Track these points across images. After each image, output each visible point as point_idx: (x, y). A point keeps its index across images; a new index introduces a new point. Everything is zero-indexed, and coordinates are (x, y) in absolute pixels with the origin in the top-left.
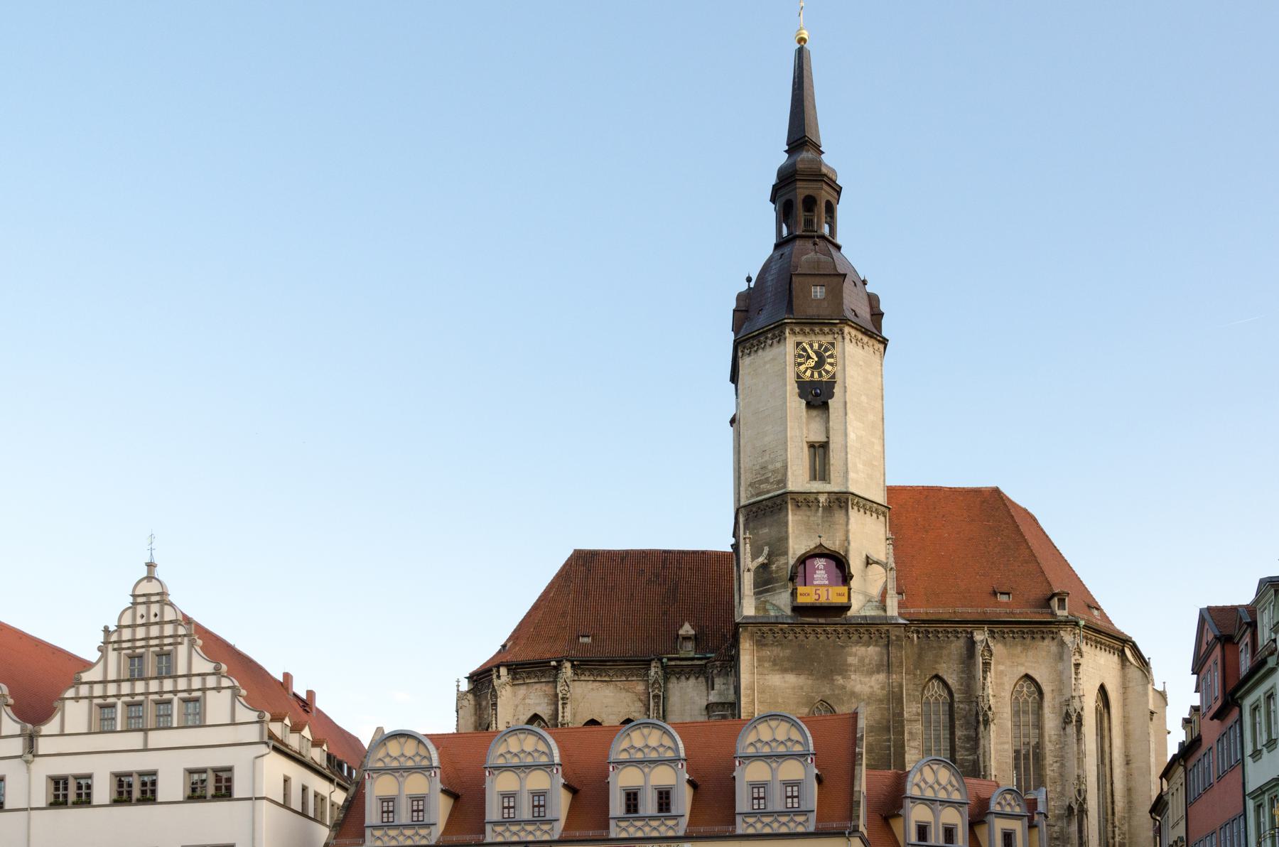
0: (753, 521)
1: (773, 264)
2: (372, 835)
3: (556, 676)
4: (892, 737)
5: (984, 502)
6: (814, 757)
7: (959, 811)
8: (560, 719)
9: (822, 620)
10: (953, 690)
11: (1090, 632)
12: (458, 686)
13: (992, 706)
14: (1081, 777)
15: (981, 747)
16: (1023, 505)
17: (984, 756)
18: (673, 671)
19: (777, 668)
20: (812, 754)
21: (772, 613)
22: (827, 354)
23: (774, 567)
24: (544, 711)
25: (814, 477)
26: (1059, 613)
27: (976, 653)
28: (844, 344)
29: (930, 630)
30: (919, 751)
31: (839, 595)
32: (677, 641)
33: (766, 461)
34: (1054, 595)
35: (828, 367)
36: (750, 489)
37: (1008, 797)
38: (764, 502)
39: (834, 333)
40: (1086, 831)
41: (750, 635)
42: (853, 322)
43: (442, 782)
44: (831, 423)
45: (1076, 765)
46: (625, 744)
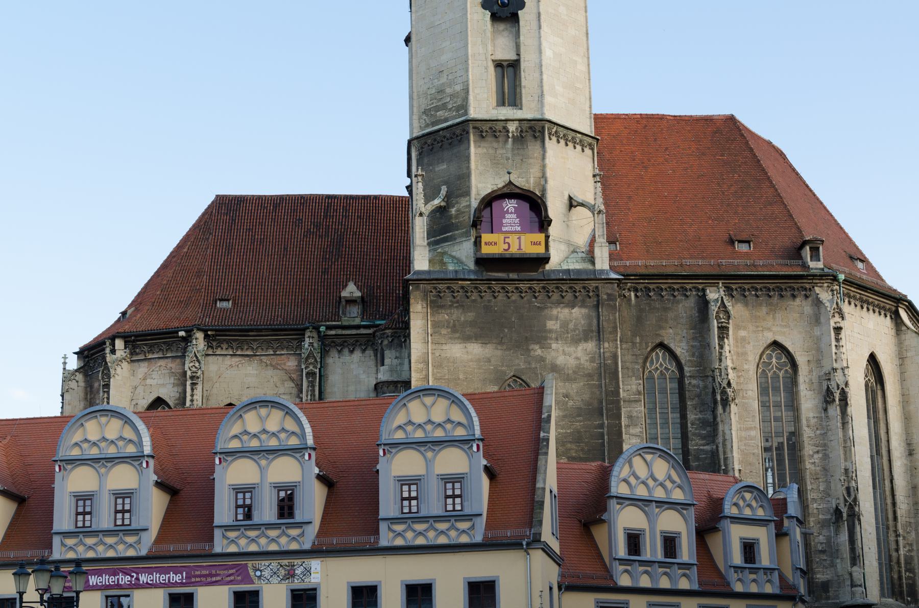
2: (63, 544)
3: (185, 350)
5: (716, 132)
9: (513, 276)
10: (683, 362)
11: (853, 289)
12: (65, 363)
13: (731, 381)
14: (850, 470)
15: (721, 433)
16: (766, 137)
17: (724, 445)
18: (333, 342)
19: (457, 335)
20: (478, 439)
21: (451, 267)
23: (453, 211)
24: (169, 393)
25: (501, 102)
26: (812, 264)
27: (710, 316)
29: (651, 286)
31: (535, 244)
32: (339, 305)
33: (443, 83)
34: (805, 243)
37: (748, 496)
38: (441, 133)
40: (859, 534)
44: (522, 38)
45: (842, 456)
46: (236, 429)
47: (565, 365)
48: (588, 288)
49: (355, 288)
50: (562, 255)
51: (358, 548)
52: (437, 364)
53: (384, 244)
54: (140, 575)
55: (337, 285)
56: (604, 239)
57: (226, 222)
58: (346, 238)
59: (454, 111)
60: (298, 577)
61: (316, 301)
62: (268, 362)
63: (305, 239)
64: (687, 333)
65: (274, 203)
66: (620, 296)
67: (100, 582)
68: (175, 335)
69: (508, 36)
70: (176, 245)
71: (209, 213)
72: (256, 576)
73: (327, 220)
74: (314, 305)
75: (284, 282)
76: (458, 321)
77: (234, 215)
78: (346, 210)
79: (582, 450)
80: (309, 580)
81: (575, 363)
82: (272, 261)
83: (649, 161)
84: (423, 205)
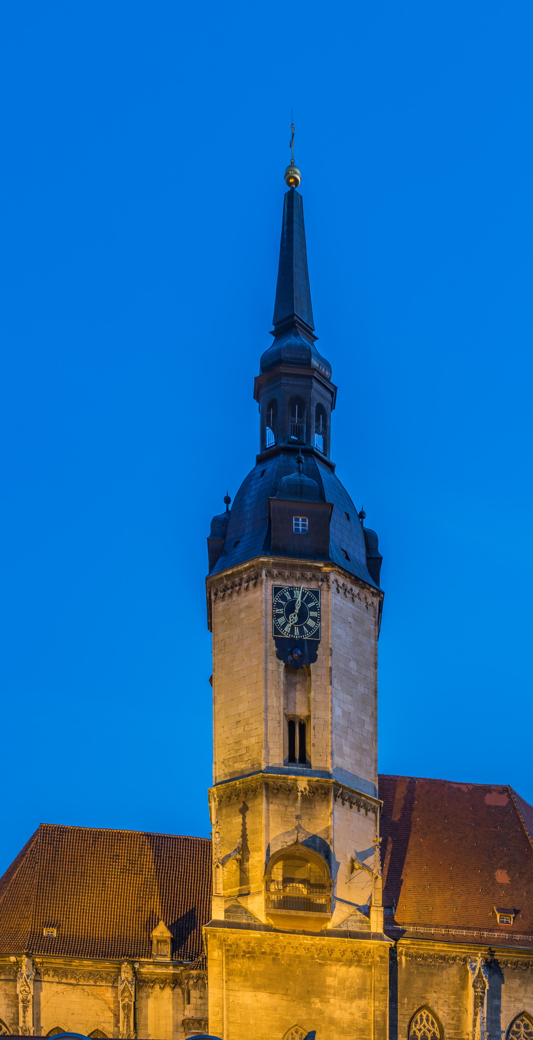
0: (227, 806)
8: (21, 1024)
10: (444, 1024)
19: (248, 984)
22: (310, 605)
35: (310, 622)
47: (341, 1019)
49: (165, 928)
62: (89, 991)
81: (350, 1017)
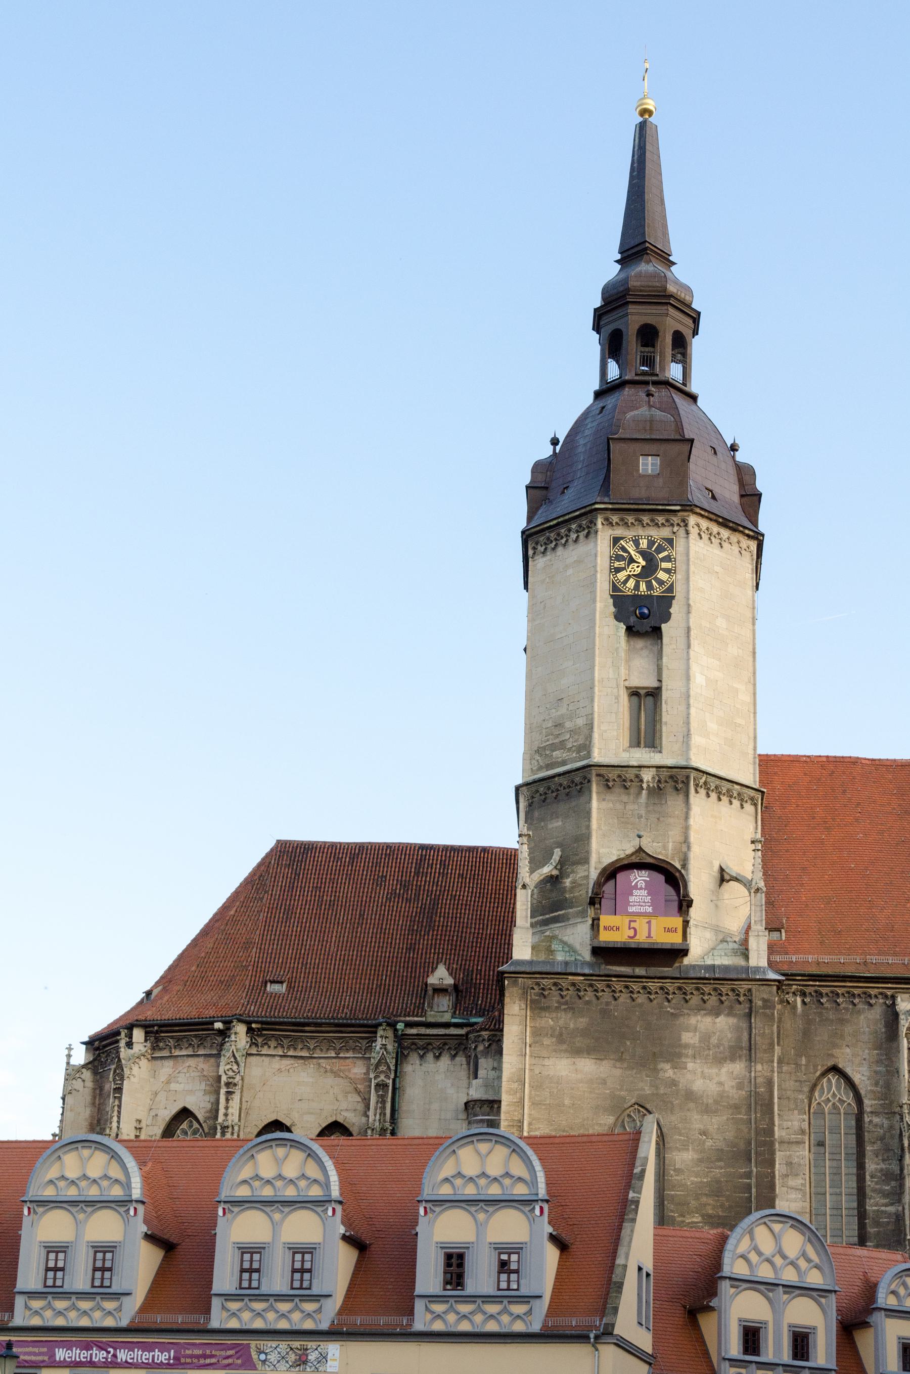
1: (588, 420)
2: (27, 1307)
4: (755, 1170)
6: (546, 1207)
7: (820, 1304)
8: (221, 1118)
9: (640, 971)
10: (863, 1092)
12: (69, 1056)
18: (413, 1044)
19: (564, 1047)
20: (542, 1200)
21: (560, 957)
22: (661, 556)
23: (567, 882)
24: (198, 1104)
25: (636, 742)
27: (900, 1033)
28: (688, 543)
29: (824, 990)
30: (804, 1195)
35: (662, 575)
36: (537, 757)
38: (556, 779)
39: (672, 525)
40: (455, 1341)
41: (520, 991)
42: (702, 509)
43: (146, 1221)
44: (665, 659)
46: (246, 1173)
48: (738, 991)
49: (446, 973)
50: (706, 946)
51: (385, 1331)
52: (536, 1084)
53: (491, 913)
54: (118, 1350)
55: (424, 967)
56: (762, 926)
57: (287, 877)
58: (442, 903)
59: (574, 751)
60: (311, 1365)
61: (395, 987)
62: (327, 1067)
63: (388, 904)
64: (869, 1054)
65: (351, 853)
66: (781, 1001)
67: (69, 1357)
68: (210, 1026)
69: (647, 656)
70: (221, 905)
71: (267, 864)
72: (260, 1360)
73: (418, 877)
74: (392, 993)
75: (356, 960)
76: (566, 1028)
77: (298, 869)
78: (445, 865)
79: (722, 1206)
80: (324, 1369)
81: (717, 1089)
82: (343, 932)
83: (834, 820)
84: (528, 874)
